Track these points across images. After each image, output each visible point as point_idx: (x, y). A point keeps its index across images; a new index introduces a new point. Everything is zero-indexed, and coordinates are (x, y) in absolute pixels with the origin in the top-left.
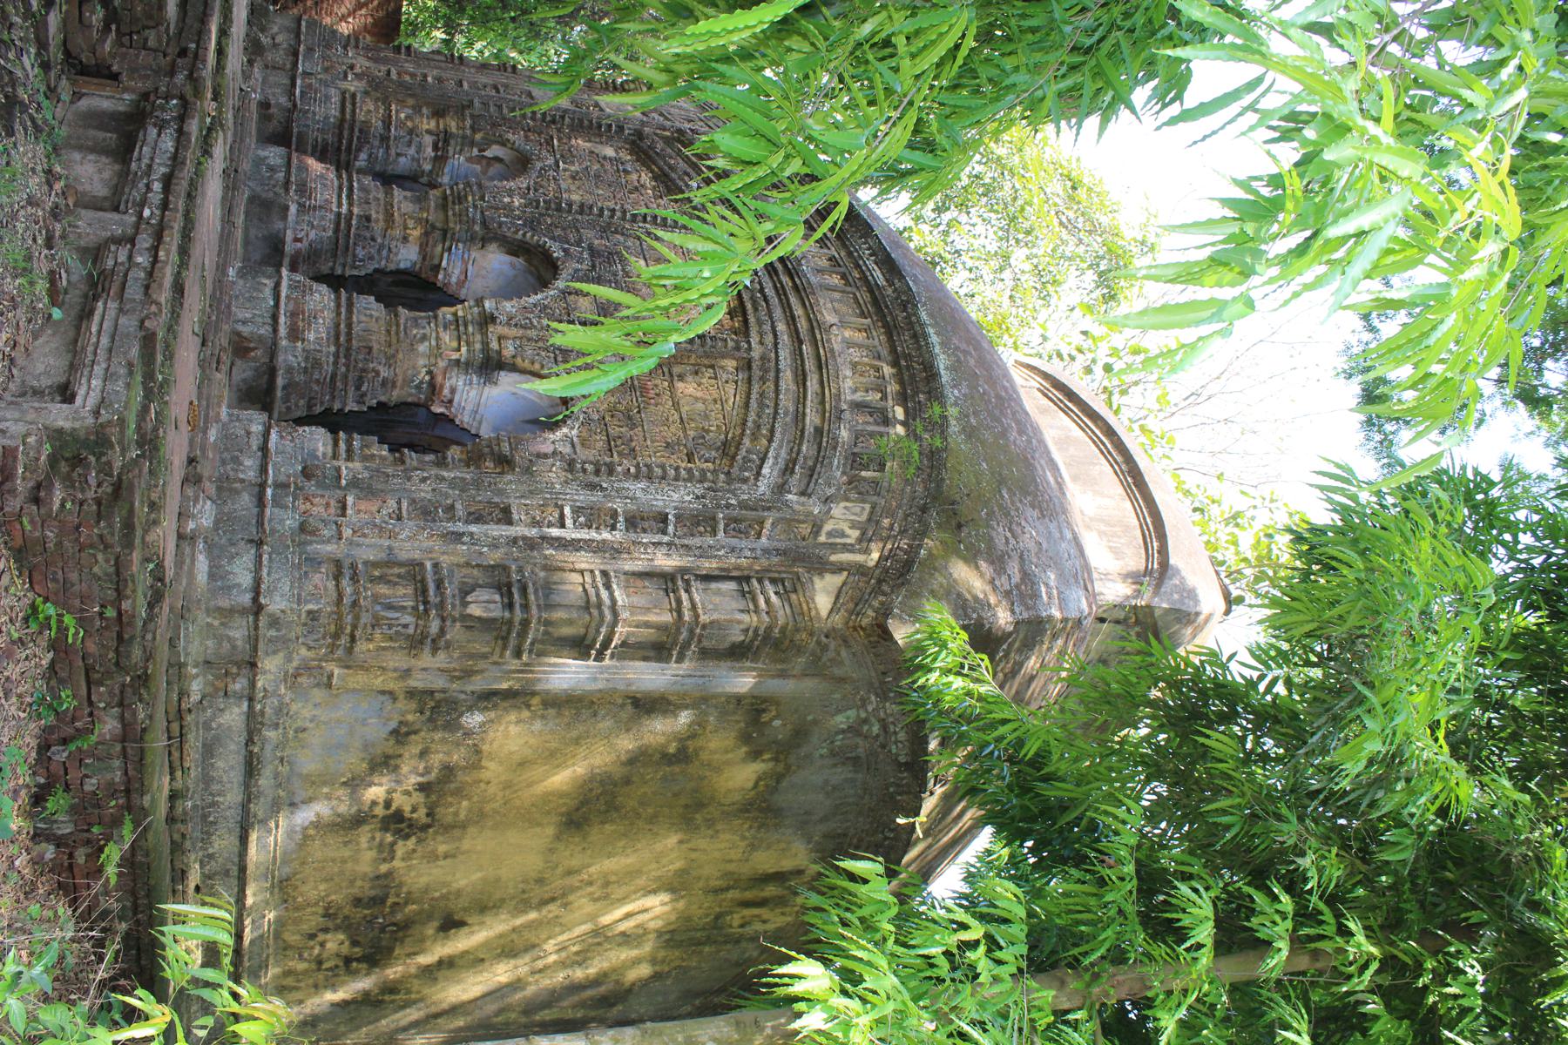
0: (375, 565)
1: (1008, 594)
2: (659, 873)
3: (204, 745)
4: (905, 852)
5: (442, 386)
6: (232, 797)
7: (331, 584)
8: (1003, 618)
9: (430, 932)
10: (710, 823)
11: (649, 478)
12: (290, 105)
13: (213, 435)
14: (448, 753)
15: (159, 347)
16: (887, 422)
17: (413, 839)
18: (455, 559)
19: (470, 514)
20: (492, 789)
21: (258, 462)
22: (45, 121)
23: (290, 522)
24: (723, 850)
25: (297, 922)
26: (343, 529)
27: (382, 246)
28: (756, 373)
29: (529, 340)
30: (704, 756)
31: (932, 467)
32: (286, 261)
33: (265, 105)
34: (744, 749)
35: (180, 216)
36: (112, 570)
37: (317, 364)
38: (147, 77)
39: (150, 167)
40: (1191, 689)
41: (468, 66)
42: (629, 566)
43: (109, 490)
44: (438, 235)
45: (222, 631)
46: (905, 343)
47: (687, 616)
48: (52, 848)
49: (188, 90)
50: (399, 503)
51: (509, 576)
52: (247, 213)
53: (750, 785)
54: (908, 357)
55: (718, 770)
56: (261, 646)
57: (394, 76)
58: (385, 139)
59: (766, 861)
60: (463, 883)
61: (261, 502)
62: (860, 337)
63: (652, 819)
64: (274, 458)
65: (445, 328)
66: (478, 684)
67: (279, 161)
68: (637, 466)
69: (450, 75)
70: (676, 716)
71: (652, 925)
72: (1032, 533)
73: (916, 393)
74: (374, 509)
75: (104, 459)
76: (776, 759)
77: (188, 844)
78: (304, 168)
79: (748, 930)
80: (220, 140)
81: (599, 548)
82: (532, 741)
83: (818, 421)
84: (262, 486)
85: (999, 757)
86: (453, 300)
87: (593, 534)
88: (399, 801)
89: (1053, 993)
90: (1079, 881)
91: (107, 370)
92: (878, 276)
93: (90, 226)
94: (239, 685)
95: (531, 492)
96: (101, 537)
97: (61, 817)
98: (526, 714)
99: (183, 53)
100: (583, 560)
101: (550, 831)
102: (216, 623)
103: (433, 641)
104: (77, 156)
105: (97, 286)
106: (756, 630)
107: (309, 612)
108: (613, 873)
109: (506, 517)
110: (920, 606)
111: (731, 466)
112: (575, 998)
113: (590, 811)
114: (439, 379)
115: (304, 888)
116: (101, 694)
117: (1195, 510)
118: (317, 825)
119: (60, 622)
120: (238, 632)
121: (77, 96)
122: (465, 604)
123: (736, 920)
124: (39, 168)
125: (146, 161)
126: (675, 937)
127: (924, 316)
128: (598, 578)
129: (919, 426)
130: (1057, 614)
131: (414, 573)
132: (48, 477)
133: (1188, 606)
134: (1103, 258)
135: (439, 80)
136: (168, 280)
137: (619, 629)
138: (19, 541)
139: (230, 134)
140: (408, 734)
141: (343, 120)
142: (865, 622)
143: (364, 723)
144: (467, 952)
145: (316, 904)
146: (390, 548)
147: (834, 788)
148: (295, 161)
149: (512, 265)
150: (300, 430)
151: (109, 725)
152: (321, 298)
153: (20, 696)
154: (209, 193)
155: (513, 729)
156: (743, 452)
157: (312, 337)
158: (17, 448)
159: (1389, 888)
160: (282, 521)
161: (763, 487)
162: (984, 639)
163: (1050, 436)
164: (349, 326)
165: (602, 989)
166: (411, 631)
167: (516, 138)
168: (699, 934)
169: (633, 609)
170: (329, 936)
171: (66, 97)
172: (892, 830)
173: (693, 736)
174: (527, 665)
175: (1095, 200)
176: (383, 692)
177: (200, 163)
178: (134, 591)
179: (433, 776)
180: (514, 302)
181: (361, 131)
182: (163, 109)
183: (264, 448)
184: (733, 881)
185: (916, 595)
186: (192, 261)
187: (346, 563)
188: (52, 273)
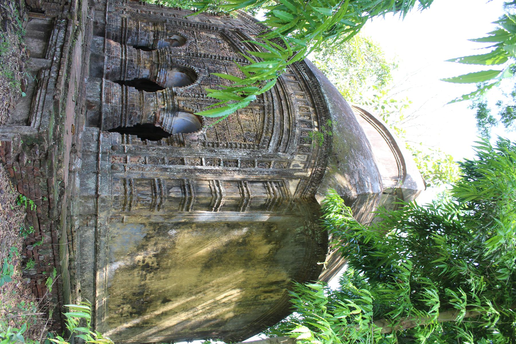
0: (137, 180)
1: (355, 185)
2: (236, 282)
3: (80, 243)
4: (320, 274)
5: (159, 118)
6: (91, 260)
7: (122, 187)
8: (354, 194)
9: (159, 303)
10: (253, 265)
11: (231, 147)
12: (104, 23)
13: (80, 136)
14: (164, 244)
15: (60, 106)
16: (311, 126)
17: (153, 273)
18: (165, 177)
19: (170, 161)
20: (179, 256)
21: (96, 145)
22: (18, 27)
23: (108, 166)
24: (258, 274)
25: (114, 301)
26: (126, 168)
27: (137, 70)
28: (266, 111)
29: (188, 101)
30: (252, 243)
31: (328, 142)
32: (104, 76)
33: (96, 23)
34: (265, 240)
35: (66, 59)
36: (45, 184)
37: (116, 111)
38: (54, 12)
39: (56, 43)
40: (424, 219)
41: (164, 8)
42: (225, 178)
43: (44, 156)
44: (157, 65)
45: (85, 204)
46: (316, 99)
47: (246, 195)
48: (29, 279)
49: (69, 16)
50: (145, 158)
51: (184, 183)
52: (90, 60)
53: (267, 252)
54: (318, 104)
55: (256, 247)
56: (99, 209)
57: (139, 12)
58: (137, 34)
59: (272, 278)
60: (169, 287)
61: (97, 159)
62: (301, 98)
63: (234, 265)
64: (101, 143)
65: (159, 97)
66: (174, 220)
67: (101, 42)
68: (227, 144)
69: (159, 11)
70: (242, 230)
71: (234, 300)
72: (362, 164)
73: (321, 117)
74: (137, 160)
75: (42, 145)
76: (276, 243)
77: (76, 276)
78: (109, 44)
79: (266, 301)
80: (80, 34)
81: (215, 172)
82: (193, 239)
83: (288, 127)
84: (98, 153)
85: (356, 243)
86: (161, 88)
87: (212, 168)
88: (147, 260)
89: (382, 328)
90: (390, 289)
91: (42, 114)
92: (306, 76)
93: (36, 64)
94: (91, 223)
95: (191, 153)
96: (41, 173)
97: (32, 269)
98: (190, 230)
99: (67, 3)
100: (209, 177)
101: (199, 269)
102: (83, 201)
103: (158, 206)
104: (30, 40)
105: (37, 85)
106: (270, 200)
107: (115, 197)
108: (220, 283)
109: (182, 162)
110: (326, 191)
111: (259, 143)
112: (208, 324)
113: (213, 262)
114: (158, 115)
115: (116, 290)
116: (44, 227)
117: (413, 155)
118: (119, 269)
119: (28, 203)
120: (91, 204)
121: (30, 19)
122: (169, 193)
123: (262, 297)
124: (16, 43)
125: (54, 41)
126: (241, 303)
127: (323, 90)
128: (215, 183)
129: (323, 128)
130: (371, 192)
131: (151, 183)
132: (22, 152)
133: (414, 188)
134: (380, 70)
135: (155, 13)
136: (63, 82)
137: (222, 200)
138: (13, 175)
139: (84, 33)
140: (150, 238)
141: (122, 27)
142: (307, 196)
143: (135, 234)
144: (171, 310)
145: (120, 295)
146: (142, 174)
147: (296, 253)
148: (106, 41)
149: (181, 75)
150: (111, 133)
151: (47, 238)
152: (117, 88)
153: (15, 229)
154: (77, 52)
155: (186, 235)
156: (263, 138)
157: (114, 101)
158: (10, 142)
159: (500, 289)
160: (105, 165)
161: (270, 150)
162: (348, 202)
163: (365, 131)
164: (126, 97)
165: (217, 321)
166: (150, 202)
167: (181, 32)
168: (250, 302)
169: (227, 193)
170: (125, 306)
171: (26, 19)
172: (315, 267)
173: (248, 236)
174: (190, 213)
175: (377, 51)
176: (141, 224)
177: (73, 42)
178: (54, 191)
179: (159, 252)
180: (183, 88)
181: (128, 31)
182: (60, 23)
183: (98, 140)
184: (262, 285)
185: (324, 186)
186: (71, 76)
187: (127, 180)
188: (22, 80)
